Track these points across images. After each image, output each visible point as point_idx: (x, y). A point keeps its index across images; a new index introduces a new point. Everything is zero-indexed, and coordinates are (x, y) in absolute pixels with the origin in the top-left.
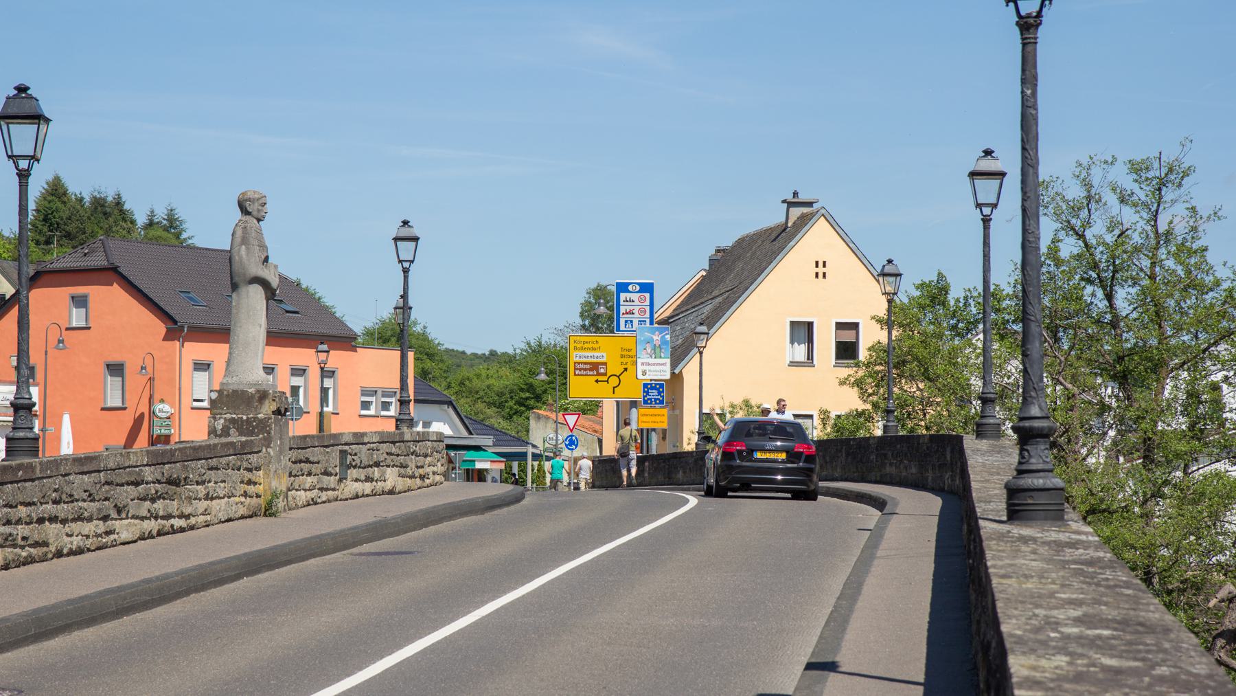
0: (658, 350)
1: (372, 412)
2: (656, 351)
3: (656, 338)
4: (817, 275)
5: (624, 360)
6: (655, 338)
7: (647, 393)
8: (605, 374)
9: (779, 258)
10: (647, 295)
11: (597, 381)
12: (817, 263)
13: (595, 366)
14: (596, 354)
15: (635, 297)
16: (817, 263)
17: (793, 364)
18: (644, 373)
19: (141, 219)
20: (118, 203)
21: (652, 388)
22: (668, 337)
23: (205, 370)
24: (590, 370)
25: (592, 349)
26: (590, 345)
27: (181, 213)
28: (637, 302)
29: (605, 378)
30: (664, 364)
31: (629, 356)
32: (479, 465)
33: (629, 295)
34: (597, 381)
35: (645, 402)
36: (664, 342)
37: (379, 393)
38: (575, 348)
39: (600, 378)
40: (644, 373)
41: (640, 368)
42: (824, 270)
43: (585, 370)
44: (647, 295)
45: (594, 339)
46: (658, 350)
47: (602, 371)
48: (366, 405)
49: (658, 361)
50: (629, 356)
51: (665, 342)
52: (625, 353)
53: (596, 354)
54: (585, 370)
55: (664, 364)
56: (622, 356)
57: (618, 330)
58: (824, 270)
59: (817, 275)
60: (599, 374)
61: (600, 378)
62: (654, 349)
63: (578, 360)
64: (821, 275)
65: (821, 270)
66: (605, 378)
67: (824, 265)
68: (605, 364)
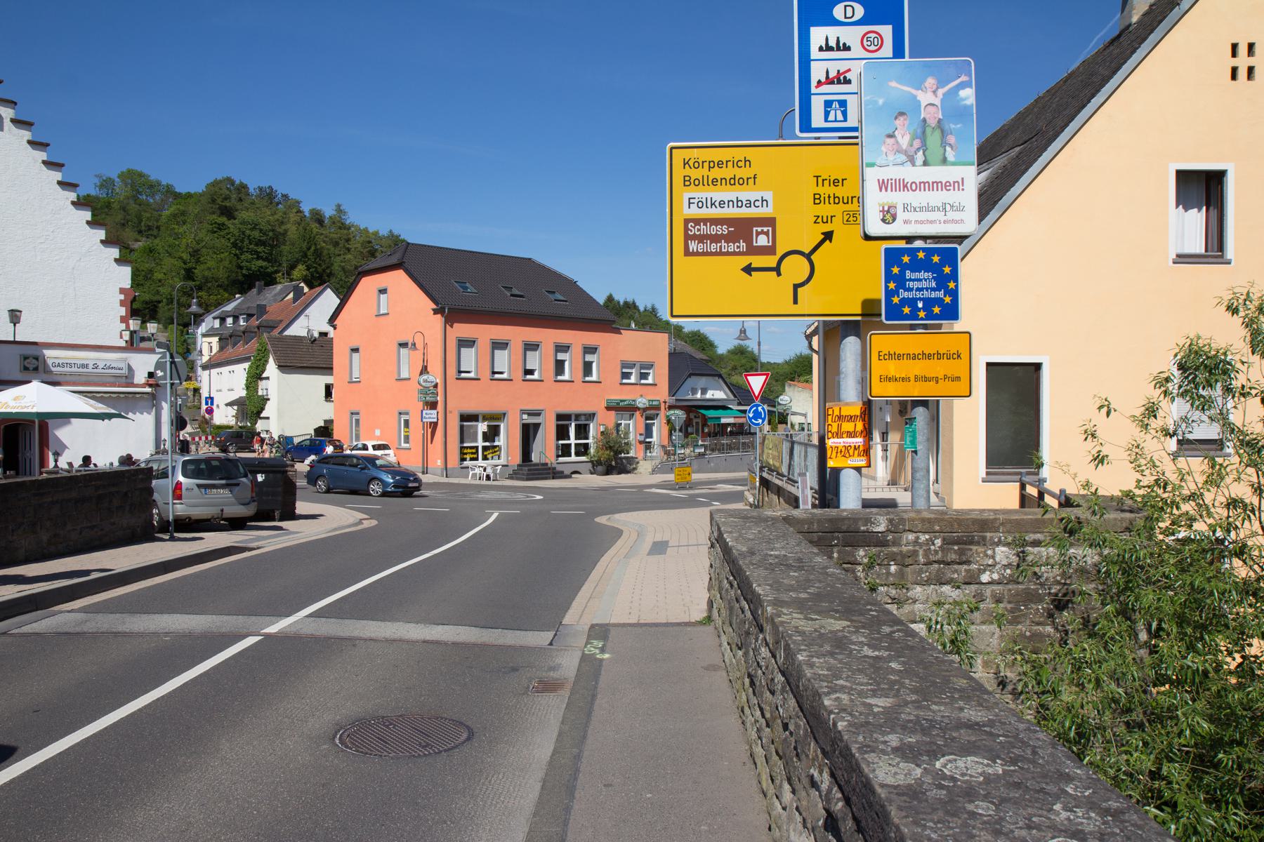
0: (934, 139)
1: (633, 380)
2: (928, 141)
3: (928, 98)
4: (1234, 73)
5: (825, 210)
6: (925, 98)
7: (901, 281)
8: (770, 250)
9: (1152, 38)
10: (886, 31)
11: (748, 270)
12: (1234, 47)
13: (741, 229)
14: (745, 195)
15: (851, 35)
16: (1234, 47)
17: (1182, 258)
18: (889, 215)
19: (642, 309)
20: (634, 303)
21: (916, 265)
22: (968, 95)
23: (472, 346)
24: (729, 238)
25: (733, 182)
26: (727, 172)
27: (657, 306)
28: (857, 51)
29: (771, 261)
30: (958, 185)
31: (836, 200)
32: (723, 421)
33: (832, 33)
34: (748, 270)
35: (894, 312)
36: (953, 110)
37: (638, 366)
38: (687, 181)
39: (758, 261)
40: (889, 215)
41: (874, 201)
42: (1251, 61)
43: (716, 239)
44: (886, 31)
45: (739, 154)
46: (934, 139)
47: (762, 241)
48: (626, 376)
49: (936, 173)
50: (836, 200)
51: (960, 113)
52: (826, 190)
53: (745, 195)
54: (716, 239)
55: (958, 185)
56: (817, 199)
57: (806, 126)
58: (1251, 61)
59: (1234, 71)
60: (754, 250)
61: (758, 261)
62: (922, 134)
63: (694, 212)
64: (1243, 73)
65: (1243, 61)
66: (771, 261)
67: (1234, 71)
68: (771, 222)
